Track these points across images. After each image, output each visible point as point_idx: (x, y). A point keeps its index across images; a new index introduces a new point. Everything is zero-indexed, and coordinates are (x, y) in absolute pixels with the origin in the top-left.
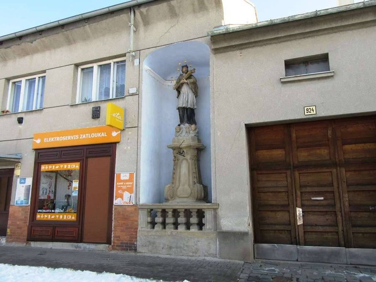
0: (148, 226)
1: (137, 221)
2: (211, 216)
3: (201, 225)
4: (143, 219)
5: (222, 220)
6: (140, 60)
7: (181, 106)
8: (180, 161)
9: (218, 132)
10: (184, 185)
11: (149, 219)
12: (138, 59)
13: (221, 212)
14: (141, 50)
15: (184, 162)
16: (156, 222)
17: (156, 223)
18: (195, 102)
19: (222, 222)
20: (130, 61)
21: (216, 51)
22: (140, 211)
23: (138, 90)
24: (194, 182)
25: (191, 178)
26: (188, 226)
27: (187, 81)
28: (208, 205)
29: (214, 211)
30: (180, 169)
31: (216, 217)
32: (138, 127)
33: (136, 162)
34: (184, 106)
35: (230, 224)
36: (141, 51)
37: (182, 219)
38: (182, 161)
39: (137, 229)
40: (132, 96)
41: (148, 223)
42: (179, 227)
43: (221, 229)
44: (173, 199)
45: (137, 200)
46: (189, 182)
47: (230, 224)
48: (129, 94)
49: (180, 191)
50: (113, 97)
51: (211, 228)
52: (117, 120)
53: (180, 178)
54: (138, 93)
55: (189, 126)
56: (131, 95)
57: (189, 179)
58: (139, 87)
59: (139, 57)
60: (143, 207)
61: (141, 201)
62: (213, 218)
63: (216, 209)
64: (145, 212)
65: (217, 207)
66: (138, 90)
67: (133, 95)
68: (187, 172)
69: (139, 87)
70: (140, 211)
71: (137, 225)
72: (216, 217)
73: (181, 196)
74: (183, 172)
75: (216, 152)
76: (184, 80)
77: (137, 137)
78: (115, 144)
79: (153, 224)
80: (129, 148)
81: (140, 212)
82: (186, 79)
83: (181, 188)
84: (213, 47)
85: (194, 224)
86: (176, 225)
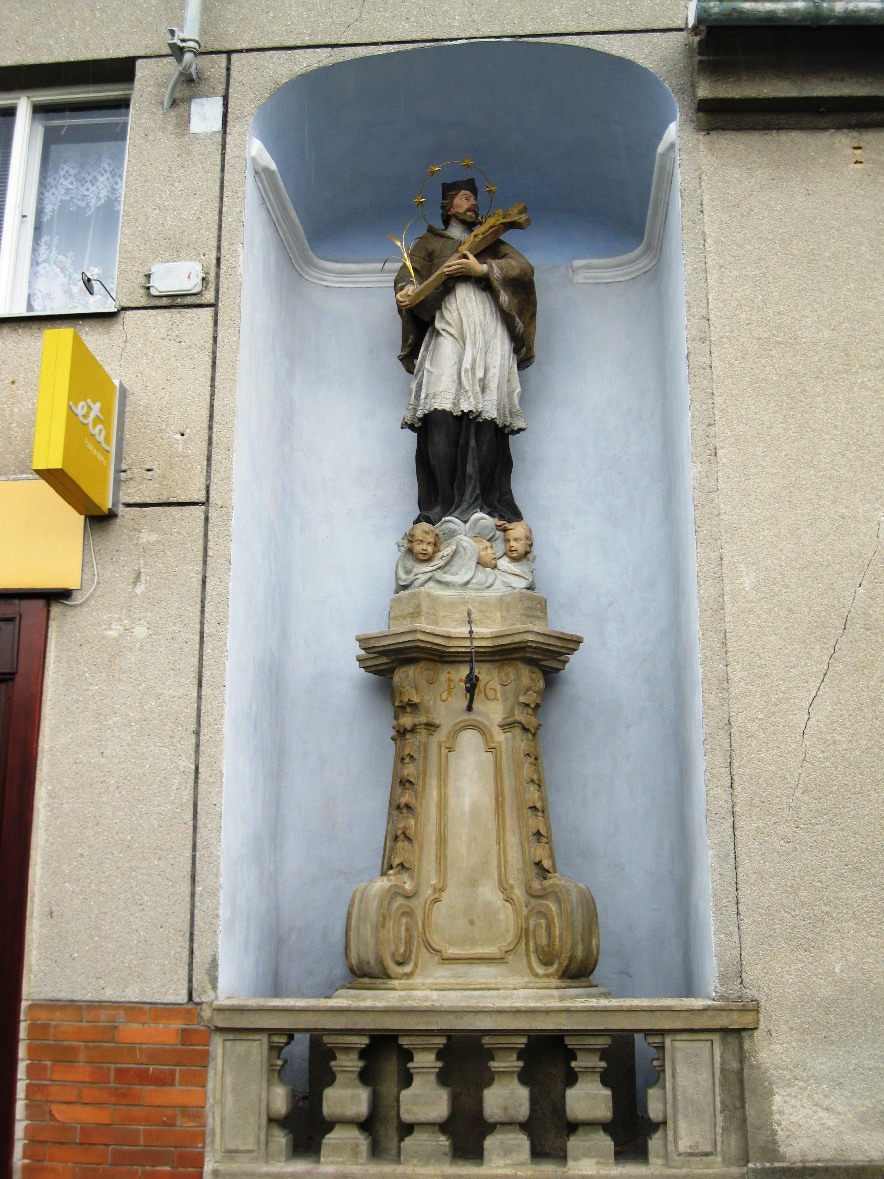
0: (273, 1146)
1: (197, 1113)
2: (705, 1075)
3: (631, 1132)
4: (235, 1097)
5: (777, 1099)
6: (226, 105)
7: (448, 407)
8: (441, 735)
9: (742, 567)
10: (473, 883)
11: (280, 1100)
12: (219, 101)
13: (771, 1052)
14: (240, 51)
15: (470, 739)
16: (491, 1120)
17: (490, 1128)
18: (519, 389)
19: (781, 1112)
20: (162, 103)
21: (717, 116)
22: (218, 1046)
23: (213, 278)
24: (538, 864)
25: (512, 839)
26: (549, 1133)
27: (484, 268)
28: (691, 1011)
29: (724, 1042)
30: (443, 783)
31: (740, 1091)
32: (205, 503)
33: (193, 727)
34: (465, 407)
35: (831, 1120)
36: (234, 56)
37: (505, 1097)
38: (454, 734)
39: (198, 1161)
40: (167, 313)
41: (272, 1120)
42: (490, 1142)
43: (771, 1150)
44: (407, 969)
45: (199, 975)
46: (502, 864)
47: (831, 1120)
48: (149, 295)
49: (446, 919)
50: (30, 307)
51: (708, 1149)
52: (90, 446)
53: (442, 841)
54: (209, 297)
55: (498, 527)
56: (165, 302)
57: (502, 852)
58: (218, 260)
59: (223, 92)
60: (236, 1027)
61: (222, 983)
62: (718, 1090)
63: (738, 1031)
64: (256, 1050)
65: (746, 1020)
66: (213, 278)
67: (175, 302)
68: (487, 802)
69: (218, 260)
70: (218, 1046)
71: (200, 1136)
72: (741, 1081)
73: (452, 951)
74: (467, 803)
75: (735, 690)
76: (465, 257)
77: (199, 568)
78: (40, 604)
79: (305, 1129)
80: (141, 631)
81: (220, 1051)
82: (480, 256)
83: (452, 896)
84: (704, 91)
85: (591, 1125)
86: (467, 1135)
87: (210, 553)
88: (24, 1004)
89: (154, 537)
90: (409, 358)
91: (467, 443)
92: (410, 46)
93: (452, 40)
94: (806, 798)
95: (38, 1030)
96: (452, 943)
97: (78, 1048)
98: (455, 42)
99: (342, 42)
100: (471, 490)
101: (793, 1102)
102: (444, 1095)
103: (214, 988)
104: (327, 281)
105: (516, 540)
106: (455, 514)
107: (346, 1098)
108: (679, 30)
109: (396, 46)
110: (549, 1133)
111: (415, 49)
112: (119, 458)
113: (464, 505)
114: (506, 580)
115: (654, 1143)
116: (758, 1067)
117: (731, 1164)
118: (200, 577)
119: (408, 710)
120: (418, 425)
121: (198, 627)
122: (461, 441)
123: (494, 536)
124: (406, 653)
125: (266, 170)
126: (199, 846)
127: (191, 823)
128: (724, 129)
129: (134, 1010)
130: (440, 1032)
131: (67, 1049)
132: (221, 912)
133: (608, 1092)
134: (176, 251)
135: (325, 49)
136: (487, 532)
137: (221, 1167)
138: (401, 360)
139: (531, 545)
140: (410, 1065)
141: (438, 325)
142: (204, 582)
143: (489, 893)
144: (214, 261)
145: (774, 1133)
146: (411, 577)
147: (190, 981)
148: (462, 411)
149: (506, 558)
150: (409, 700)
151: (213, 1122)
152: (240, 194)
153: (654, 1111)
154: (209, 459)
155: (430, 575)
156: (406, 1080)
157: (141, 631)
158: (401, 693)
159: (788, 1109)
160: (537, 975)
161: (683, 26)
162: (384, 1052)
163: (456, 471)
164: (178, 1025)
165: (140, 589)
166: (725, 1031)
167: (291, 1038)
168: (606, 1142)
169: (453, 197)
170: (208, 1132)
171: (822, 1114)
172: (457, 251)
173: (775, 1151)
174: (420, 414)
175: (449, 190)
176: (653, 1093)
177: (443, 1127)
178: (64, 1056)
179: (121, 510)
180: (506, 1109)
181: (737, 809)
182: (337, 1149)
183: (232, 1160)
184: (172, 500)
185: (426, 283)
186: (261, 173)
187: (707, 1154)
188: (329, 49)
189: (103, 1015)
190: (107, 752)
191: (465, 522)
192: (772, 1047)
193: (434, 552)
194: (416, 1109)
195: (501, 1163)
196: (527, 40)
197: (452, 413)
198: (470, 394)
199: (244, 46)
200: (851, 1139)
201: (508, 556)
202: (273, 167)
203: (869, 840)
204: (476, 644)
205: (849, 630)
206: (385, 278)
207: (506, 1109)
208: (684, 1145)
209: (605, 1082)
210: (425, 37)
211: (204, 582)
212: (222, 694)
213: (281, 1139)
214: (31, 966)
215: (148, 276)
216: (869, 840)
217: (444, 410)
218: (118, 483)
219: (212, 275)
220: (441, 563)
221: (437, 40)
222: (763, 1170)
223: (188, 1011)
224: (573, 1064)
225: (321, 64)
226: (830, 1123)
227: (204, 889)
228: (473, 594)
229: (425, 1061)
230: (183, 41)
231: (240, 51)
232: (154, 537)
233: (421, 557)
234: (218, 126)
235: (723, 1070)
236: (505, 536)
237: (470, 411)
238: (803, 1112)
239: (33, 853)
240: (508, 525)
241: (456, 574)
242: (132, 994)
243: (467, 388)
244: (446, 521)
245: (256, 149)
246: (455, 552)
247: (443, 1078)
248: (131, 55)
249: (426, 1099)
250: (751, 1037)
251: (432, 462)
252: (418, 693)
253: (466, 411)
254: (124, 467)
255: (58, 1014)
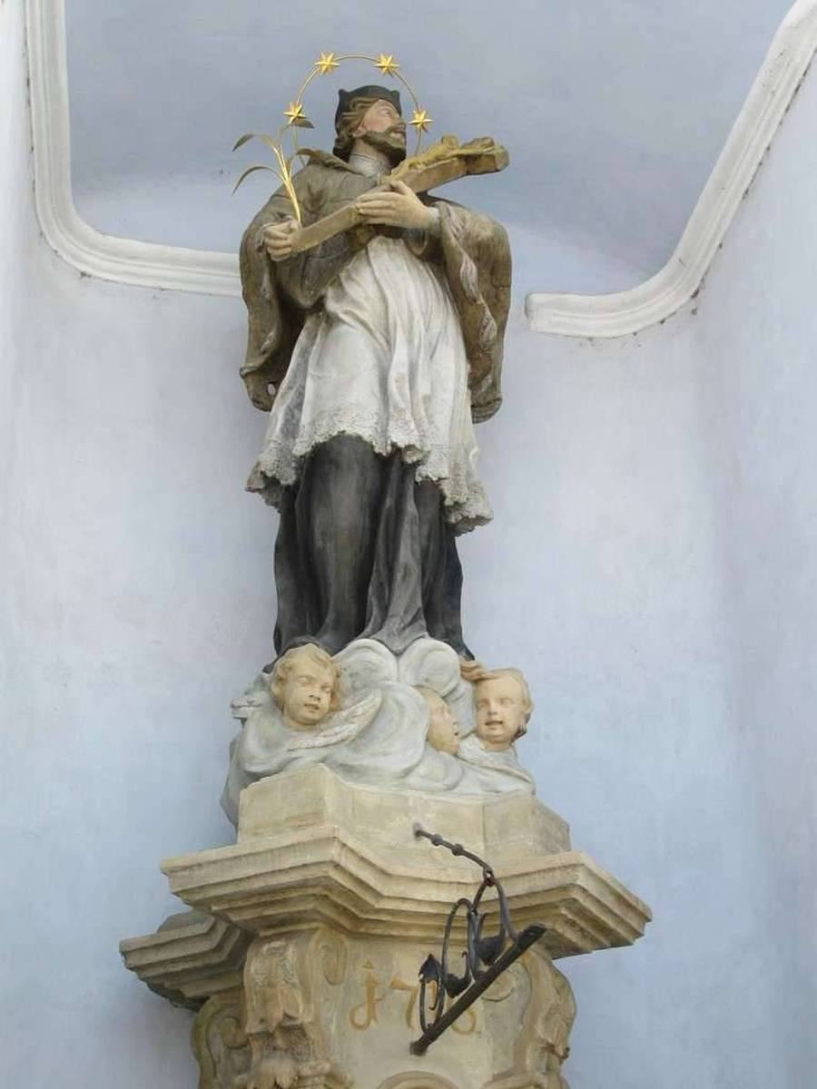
90: (268, 371)
91: (399, 510)
104: (87, 263)
105: (502, 701)
113: (394, 624)
114: (482, 777)
119: (280, 1042)
120: (289, 478)
122: (389, 502)
123: (455, 689)
124: (285, 902)
136: (445, 678)
138: (244, 377)
139: (527, 718)
146: (282, 755)
148: (394, 445)
149: (474, 739)
150: (287, 1016)
155: (324, 752)
158: (265, 1001)
174: (301, 447)
185: (308, 228)
191: (398, 655)
193: (333, 710)
197: (372, 447)
198: (408, 416)
201: (480, 736)
206: (195, 276)
217: (359, 438)
220: (351, 729)
227: (342, 250)
233: (307, 714)
236: (475, 693)
237: (409, 447)
243: (402, 405)
244: (358, 648)
246: (380, 711)
251: (319, 543)
252: (307, 1000)
253: (401, 445)
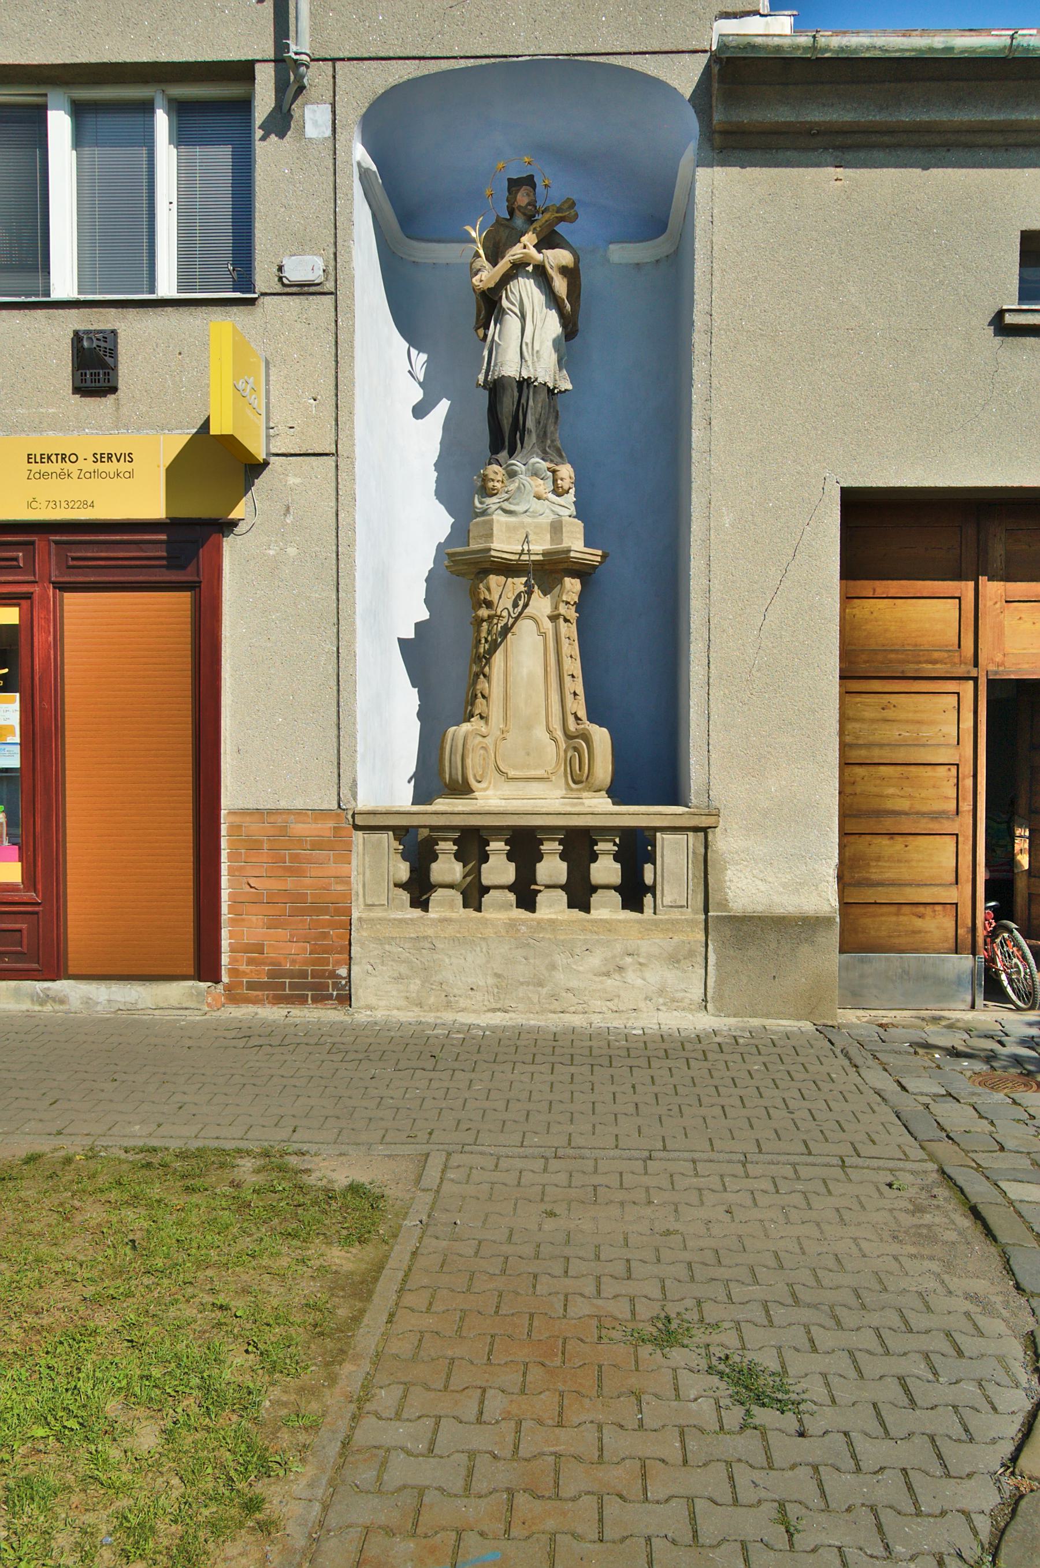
1: (345, 880)
3: (634, 893)
14: (343, 60)
37: (552, 868)
43: (723, 905)
45: (345, 791)
47: (762, 886)
48: (284, 285)
54: (329, 286)
58: (335, 254)
67: (304, 289)
69: (335, 254)
71: (347, 896)
77: (333, 504)
79: (419, 890)
80: (292, 551)
87: (340, 493)
88: (223, 812)
89: (298, 481)
92: (484, 61)
93: (518, 56)
94: (759, 674)
95: (234, 829)
96: (515, 768)
97: (263, 841)
98: (520, 59)
99: (428, 55)
100: (532, 439)
101: (739, 874)
102: (512, 866)
103: (355, 799)
106: (518, 458)
107: (447, 868)
108: (705, 51)
109: (472, 60)
110: (580, 893)
111: (487, 64)
112: (268, 419)
115: (648, 899)
116: (716, 852)
117: (697, 913)
118: (334, 510)
121: (334, 547)
125: (367, 170)
126: (342, 704)
127: (335, 688)
128: (734, 148)
129: (300, 813)
130: (508, 827)
131: (256, 841)
132: (358, 749)
133: (618, 866)
134: (302, 246)
135: (413, 62)
137: (364, 915)
140: (487, 848)
141: (505, 303)
142: (337, 515)
143: (540, 733)
144: (332, 256)
145: (726, 894)
147: (339, 794)
151: (357, 886)
152: (350, 196)
153: (648, 880)
154: (337, 420)
156: (485, 858)
157: (292, 551)
159: (735, 879)
160: (572, 790)
161: (708, 48)
162: (472, 842)
163: (518, 428)
164: (331, 824)
165: (289, 520)
166: (696, 829)
167: (407, 831)
168: (617, 898)
169: (517, 193)
170: (353, 892)
171: (759, 883)
172: (519, 241)
173: (726, 905)
175: (514, 185)
176: (648, 868)
177: (510, 888)
178: (254, 846)
179: (273, 459)
180: (551, 876)
181: (711, 681)
182: (441, 904)
183: (370, 910)
184: (310, 451)
186: (364, 175)
187: (682, 907)
188: (417, 61)
189: (280, 820)
190: (273, 638)
192: (727, 839)
194: (491, 876)
195: (547, 911)
196: (579, 58)
199: (347, 55)
200: (776, 899)
202: (374, 168)
203: (800, 704)
204: (533, 558)
205: (798, 556)
207: (551, 876)
208: (667, 900)
209: (616, 859)
210: (496, 53)
211: (337, 515)
212: (354, 598)
213: (405, 896)
214: (226, 786)
215: (280, 269)
216: (800, 704)
218: (268, 437)
219: (331, 269)
221: (505, 56)
222: (717, 916)
223: (338, 815)
224: (596, 848)
225: (411, 77)
226: (762, 888)
228: (529, 520)
229: (497, 846)
230: (296, 54)
231: (343, 60)
232: (298, 481)
234: (328, 133)
235: (694, 853)
238: (745, 881)
239: (223, 709)
240: (557, 468)
241: (518, 504)
242: (299, 804)
245: (360, 153)
247: (510, 857)
248: (250, 58)
249: (499, 869)
250: (714, 833)
254: (272, 425)
255: (248, 819)
